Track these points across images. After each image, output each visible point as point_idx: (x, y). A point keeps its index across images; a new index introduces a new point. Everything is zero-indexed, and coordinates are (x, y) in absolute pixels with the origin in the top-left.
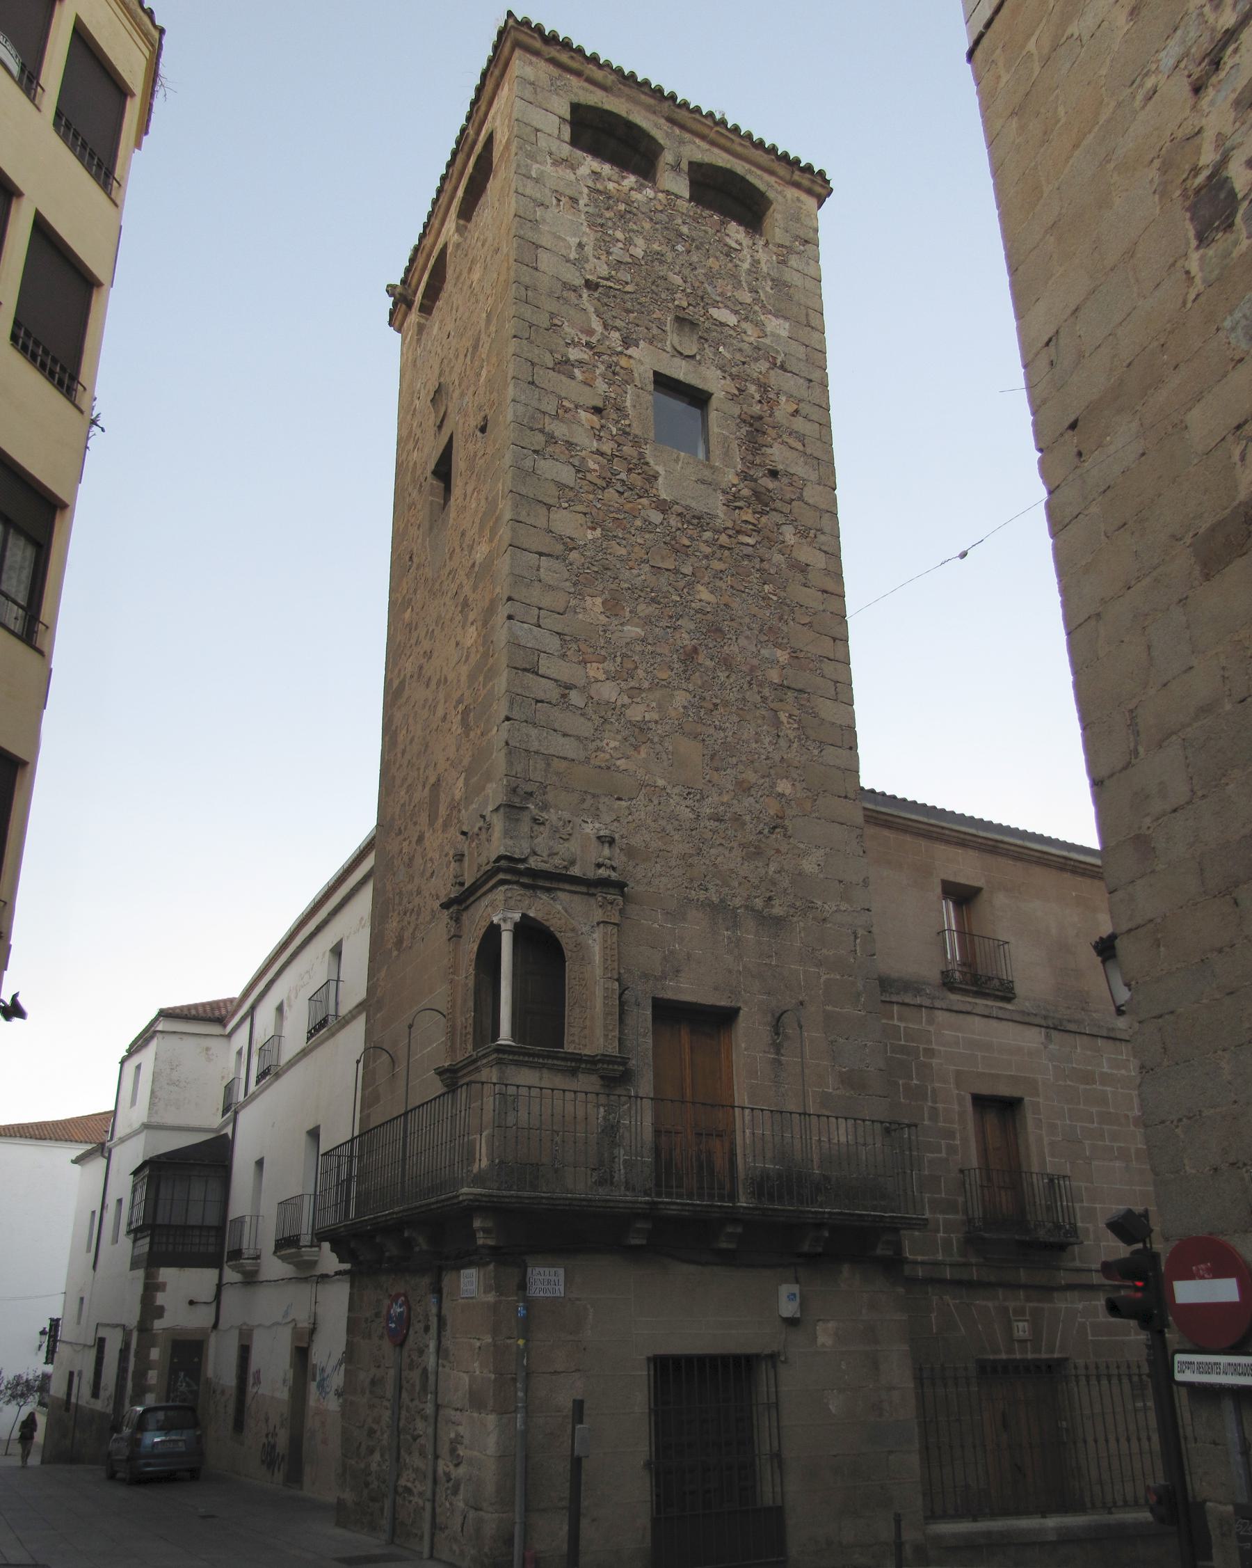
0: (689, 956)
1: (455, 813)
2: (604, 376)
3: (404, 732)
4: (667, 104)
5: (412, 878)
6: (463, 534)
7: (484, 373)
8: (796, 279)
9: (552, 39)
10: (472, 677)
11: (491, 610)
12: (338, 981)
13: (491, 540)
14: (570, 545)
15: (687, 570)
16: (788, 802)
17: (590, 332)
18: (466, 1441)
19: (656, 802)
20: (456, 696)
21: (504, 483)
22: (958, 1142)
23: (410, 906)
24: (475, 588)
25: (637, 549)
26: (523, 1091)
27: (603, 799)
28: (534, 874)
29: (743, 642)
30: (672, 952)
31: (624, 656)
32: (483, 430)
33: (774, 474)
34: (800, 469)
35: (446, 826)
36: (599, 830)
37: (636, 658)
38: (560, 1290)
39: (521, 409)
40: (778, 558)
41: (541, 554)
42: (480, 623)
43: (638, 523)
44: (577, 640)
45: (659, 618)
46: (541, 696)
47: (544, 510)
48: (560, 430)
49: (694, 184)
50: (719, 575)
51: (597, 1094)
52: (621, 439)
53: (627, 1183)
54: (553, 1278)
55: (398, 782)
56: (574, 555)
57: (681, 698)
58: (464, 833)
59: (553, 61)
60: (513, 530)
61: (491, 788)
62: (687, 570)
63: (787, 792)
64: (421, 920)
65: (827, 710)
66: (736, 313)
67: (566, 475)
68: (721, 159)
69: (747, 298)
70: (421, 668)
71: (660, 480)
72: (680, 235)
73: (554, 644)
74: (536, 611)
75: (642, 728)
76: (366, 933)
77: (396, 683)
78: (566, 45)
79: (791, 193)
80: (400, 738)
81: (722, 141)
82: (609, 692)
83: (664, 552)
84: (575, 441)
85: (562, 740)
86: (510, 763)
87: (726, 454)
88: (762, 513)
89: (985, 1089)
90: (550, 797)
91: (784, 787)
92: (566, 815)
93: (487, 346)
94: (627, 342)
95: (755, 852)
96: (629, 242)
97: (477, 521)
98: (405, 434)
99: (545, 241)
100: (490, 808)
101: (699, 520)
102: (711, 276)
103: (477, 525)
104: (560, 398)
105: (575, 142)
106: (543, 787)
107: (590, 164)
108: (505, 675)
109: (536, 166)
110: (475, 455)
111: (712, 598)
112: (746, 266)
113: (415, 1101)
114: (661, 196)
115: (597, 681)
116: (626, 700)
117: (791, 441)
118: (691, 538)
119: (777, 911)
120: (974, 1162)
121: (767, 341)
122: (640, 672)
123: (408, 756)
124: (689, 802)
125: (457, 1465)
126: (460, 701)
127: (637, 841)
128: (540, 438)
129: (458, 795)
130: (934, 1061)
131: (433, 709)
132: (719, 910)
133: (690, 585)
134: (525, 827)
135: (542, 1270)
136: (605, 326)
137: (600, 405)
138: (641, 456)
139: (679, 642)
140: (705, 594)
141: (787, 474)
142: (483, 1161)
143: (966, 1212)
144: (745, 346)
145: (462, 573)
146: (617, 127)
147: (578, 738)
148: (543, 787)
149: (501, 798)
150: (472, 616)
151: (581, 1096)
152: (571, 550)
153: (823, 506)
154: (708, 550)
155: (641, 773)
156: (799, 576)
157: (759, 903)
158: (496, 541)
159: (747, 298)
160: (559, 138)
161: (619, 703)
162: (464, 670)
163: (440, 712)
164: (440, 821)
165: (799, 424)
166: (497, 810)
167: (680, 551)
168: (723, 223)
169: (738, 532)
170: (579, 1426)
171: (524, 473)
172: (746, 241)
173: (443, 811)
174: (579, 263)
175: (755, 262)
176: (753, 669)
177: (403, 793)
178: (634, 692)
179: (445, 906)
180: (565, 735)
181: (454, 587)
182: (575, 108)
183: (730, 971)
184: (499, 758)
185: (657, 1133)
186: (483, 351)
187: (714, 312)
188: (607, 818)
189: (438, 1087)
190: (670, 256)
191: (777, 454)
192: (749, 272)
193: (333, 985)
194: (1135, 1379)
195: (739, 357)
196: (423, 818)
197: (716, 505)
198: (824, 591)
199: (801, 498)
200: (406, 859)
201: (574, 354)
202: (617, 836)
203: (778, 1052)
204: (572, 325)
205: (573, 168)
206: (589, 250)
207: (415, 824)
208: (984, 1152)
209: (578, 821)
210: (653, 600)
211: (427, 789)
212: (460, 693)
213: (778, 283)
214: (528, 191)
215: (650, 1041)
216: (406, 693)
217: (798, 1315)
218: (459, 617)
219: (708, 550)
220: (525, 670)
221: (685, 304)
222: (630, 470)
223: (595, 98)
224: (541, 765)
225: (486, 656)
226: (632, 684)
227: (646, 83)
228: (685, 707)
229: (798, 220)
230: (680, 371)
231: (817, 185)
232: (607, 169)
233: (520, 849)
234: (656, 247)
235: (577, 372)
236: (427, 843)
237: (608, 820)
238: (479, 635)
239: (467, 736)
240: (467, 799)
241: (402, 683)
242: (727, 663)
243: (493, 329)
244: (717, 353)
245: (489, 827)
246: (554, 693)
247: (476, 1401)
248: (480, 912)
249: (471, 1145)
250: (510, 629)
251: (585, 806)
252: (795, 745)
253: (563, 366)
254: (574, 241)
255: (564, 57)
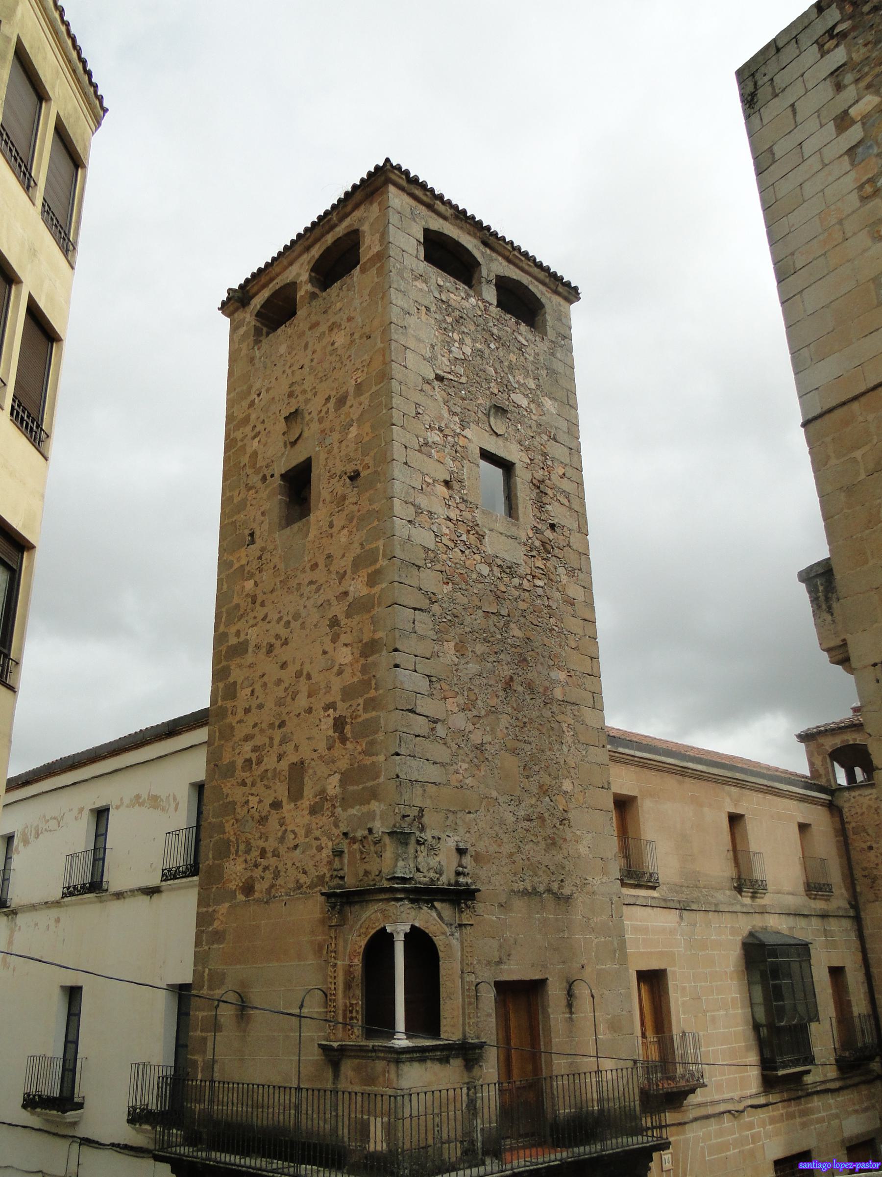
9: (415, 181)
78: (423, 186)
255: (419, 193)
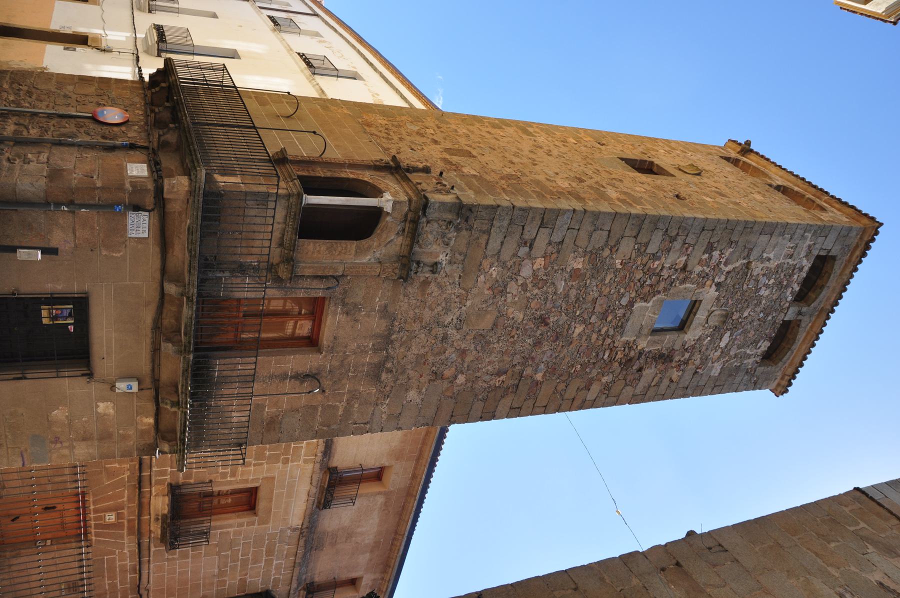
0: (356, 321)
1: (453, 167)
2: (703, 271)
3: (502, 134)
4: (829, 307)
5: (409, 135)
6: (621, 181)
7: (708, 199)
8: (738, 379)
10: (538, 183)
11: (578, 198)
12: (338, 76)
13: (618, 199)
14: (614, 249)
15: (593, 319)
16: (451, 382)
17: (726, 264)
18: (26, 166)
19: (457, 300)
20: (526, 171)
21: (651, 211)
22: (229, 479)
23: (391, 133)
24: (591, 187)
25: (608, 290)
26: (270, 213)
27: (460, 266)
28: (415, 222)
29: (549, 353)
30: (360, 310)
31: (546, 281)
32: (677, 196)
33: (640, 370)
34: (643, 383)
35: (445, 160)
36: (441, 264)
37: (545, 288)
38: (132, 234)
39: (690, 222)
40: (595, 372)
41: (610, 231)
42: (570, 190)
43: (622, 291)
44: (558, 252)
45: (567, 302)
46: (527, 228)
47: (634, 234)
48: (677, 245)
49: (790, 322)
50: (589, 337)
51: (268, 262)
52: (668, 282)
53: (206, 279)
54: (141, 229)
55: (471, 128)
56: (607, 252)
57: (520, 316)
58: (441, 174)
59: (857, 246)
60: (625, 214)
61: (471, 194)
62: (593, 319)
63: (458, 381)
64: (384, 140)
65: (506, 402)
66: (726, 347)
67: (652, 249)
68: (801, 336)
69: (732, 353)
70: (541, 147)
71: (644, 304)
72: (767, 316)
73: (556, 238)
74: (577, 227)
75: (503, 292)
76: (368, 99)
77: (531, 130)
78: (864, 255)
79: (779, 374)
80: (498, 131)
81: (809, 338)
82: (526, 272)
83: (604, 306)
84: (671, 253)
85: (499, 242)
86: (487, 207)
87: (655, 342)
88: (620, 364)
89: (261, 494)
90: (464, 233)
91: (461, 379)
92: (452, 243)
93: (722, 201)
94: (718, 285)
95: (421, 360)
96: (767, 286)
97: (629, 191)
98: (673, 145)
99: (774, 240)
100: (458, 193)
101: (620, 328)
102: (746, 332)
103: (625, 190)
104: (694, 246)
105: (818, 257)
106: (470, 229)
107: (807, 265)
108: (540, 206)
109: (810, 235)
110: (665, 191)
111: (575, 335)
112: (748, 352)
113: (261, 132)
114: (787, 304)
115: (533, 264)
116: (520, 282)
117: (656, 379)
118: (611, 321)
119: (384, 376)
120: (216, 489)
121: (710, 364)
122: (536, 291)
123: (487, 136)
124: (455, 321)
125: (9, 160)
126: (523, 174)
127: (433, 287)
128: (674, 234)
129: (465, 170)
130: (280, 464)
131: (516, 155)
132: (386, 340)
133: (584, 322)
134: (449, 216)
135: (147, 222)
136: (728, 273)
137: (688, 269)
138: (659, 292)
139: (552, 314)
140: (579, 329)
141: (641, 376)
142: (222, 180)
143: (184, 484)
144: (709, 352)
145: (599, 179)
146: (822, 280)
147: (499, 251)
148: (470, 229)
149: (465, 201)
150: (574, 184)
151: (266, 251)
152: (611, 250)
153: (621, 397)
154: (603, 331)
155: (475, 291)
156: (583, 385)
157: (389, 365)
158: (618, 203)
159: (732, 353)
160: (821, 249)
161: (518, 278)
162: (541, 178)
163: (515, 160)
164: (448, 157)
165: (666, 382)
166: (458, 198)
167: (604, 316)
168: (770, 338)
169: (611, 350)
170: (39, 252)
171: (656, 221)
172: (759, 352)
173: (455, 159)
174: (761, 259)
175: (749, 356)
176: (533, 359)
177: (464, 131)
178: (524, 287)
179: (394, 158)
180: (502, 243)
181: (590, 173)
182: (834, 258)
183: (346, 347)
184: (489, 200)
185: (239, 300)
186: (719, 199)
187: (728, 334)
188: (448, 269)
189: (272, 151)
190: (758, 309)
191: (649, 373)
192: (745, 353)
193: (335, 73)
194: (80, 583)
195: (704, 348)
196: (449, 145)
197: (628, 337)
198: (573, 399)
199: (626, 385)
200: (422, 131)
201: (716, 254)
202: (436, 275)
203: (292, 377)
204: (731, 254)
205: (806, 256)
206: (767, 264)
207: (445, 139)
208: (219, 494)
209: (448, 251)
210: (578, 299)
211: (468, 148)
212: (528, 174)
213: (738, 368)
214: (798, 231)
215: (301, 296)
216: (524, 136)
217: (117, 391)
218: (572, 175)
219: (603, 331)
220: (543, 219)
221: (734, 318)
222: (651, 286)
223: (838, 268)
224: (485, 228)
225: (552, 193)
226: (530, 286)
227: (841, 297)
228: (513, 318)
229: (766, 379)
230: (701, 315)
231: (781, 390)
232: (804, 275)
233: (432, 213)
234: (764, 302)
235: (707, 256)
236: (434, 146)
237: (447, 270)
238: (563, 189)
239: (502, 178)
240: (463, 176)
241: (529, 134)
242: (538, 343)
243: (731, 206)
244: (707, 336)
245: (448, 192)
246: (527, 236)
247: (55, 174)
248: (391, 184)
249: (233, 174)
250: (568, 210)
251: (457, 255)
252: (486, 385)
253: (710, 249)
254: (771, 256)
255: (858, 253)
